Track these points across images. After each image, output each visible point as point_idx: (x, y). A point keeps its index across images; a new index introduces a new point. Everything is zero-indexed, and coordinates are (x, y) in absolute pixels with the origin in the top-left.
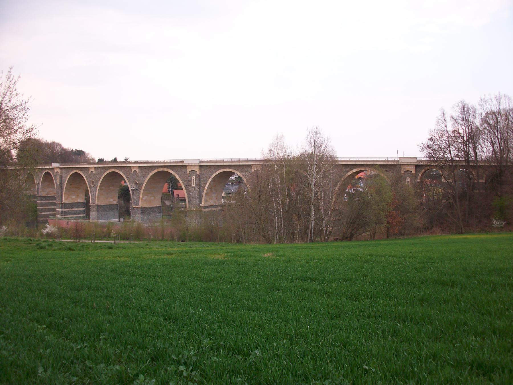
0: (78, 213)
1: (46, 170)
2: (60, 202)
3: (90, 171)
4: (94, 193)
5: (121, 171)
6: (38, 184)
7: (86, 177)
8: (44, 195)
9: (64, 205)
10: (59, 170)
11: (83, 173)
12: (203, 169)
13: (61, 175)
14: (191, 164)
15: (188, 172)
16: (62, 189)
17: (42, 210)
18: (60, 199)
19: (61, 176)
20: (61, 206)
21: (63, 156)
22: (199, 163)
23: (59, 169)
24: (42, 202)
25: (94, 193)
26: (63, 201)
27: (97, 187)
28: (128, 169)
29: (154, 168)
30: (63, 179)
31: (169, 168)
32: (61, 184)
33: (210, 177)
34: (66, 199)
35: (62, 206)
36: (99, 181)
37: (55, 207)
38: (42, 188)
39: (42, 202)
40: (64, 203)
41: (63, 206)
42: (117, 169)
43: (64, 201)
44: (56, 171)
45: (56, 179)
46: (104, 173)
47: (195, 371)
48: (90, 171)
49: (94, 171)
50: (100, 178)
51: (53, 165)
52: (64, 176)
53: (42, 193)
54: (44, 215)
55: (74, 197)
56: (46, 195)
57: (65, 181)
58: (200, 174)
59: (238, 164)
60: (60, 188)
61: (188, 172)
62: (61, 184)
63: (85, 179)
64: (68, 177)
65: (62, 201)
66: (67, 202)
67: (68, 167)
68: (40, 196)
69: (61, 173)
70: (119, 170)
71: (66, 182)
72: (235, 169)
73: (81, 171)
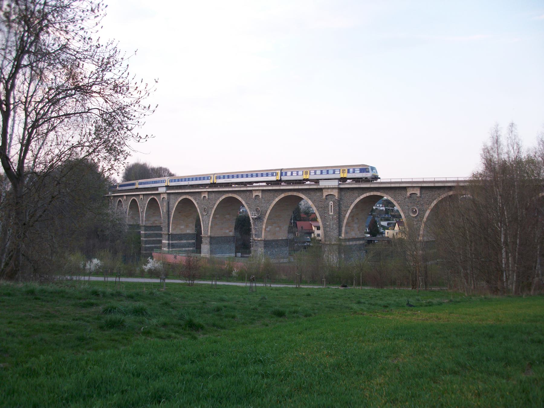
7: (197, 203)
8: (148, 225)
11: (193, 198)
12: (343, 193)
15: (324, 197)
17: (147, 242)
24: (146, 232)
27: (210, 216)
30: (171, 206)
31: (299, 192)
32: (168, 212)
34: (173, 229)
39: (146, 232)
40: (172, 234)
41: (170, 237)
42: (234, 193)
45: (162, 206)
46: (219, 198)
50: (215, 204)
54: (149, 247)
55: (182, 227)
56: (151, 225)
58: (339, 199)
60: (167, 217)
62: (168, 212)
63: (196, 206)
64: (177, 204)
66: (175, 232)
69: (169, 199)
71: (174, 209)
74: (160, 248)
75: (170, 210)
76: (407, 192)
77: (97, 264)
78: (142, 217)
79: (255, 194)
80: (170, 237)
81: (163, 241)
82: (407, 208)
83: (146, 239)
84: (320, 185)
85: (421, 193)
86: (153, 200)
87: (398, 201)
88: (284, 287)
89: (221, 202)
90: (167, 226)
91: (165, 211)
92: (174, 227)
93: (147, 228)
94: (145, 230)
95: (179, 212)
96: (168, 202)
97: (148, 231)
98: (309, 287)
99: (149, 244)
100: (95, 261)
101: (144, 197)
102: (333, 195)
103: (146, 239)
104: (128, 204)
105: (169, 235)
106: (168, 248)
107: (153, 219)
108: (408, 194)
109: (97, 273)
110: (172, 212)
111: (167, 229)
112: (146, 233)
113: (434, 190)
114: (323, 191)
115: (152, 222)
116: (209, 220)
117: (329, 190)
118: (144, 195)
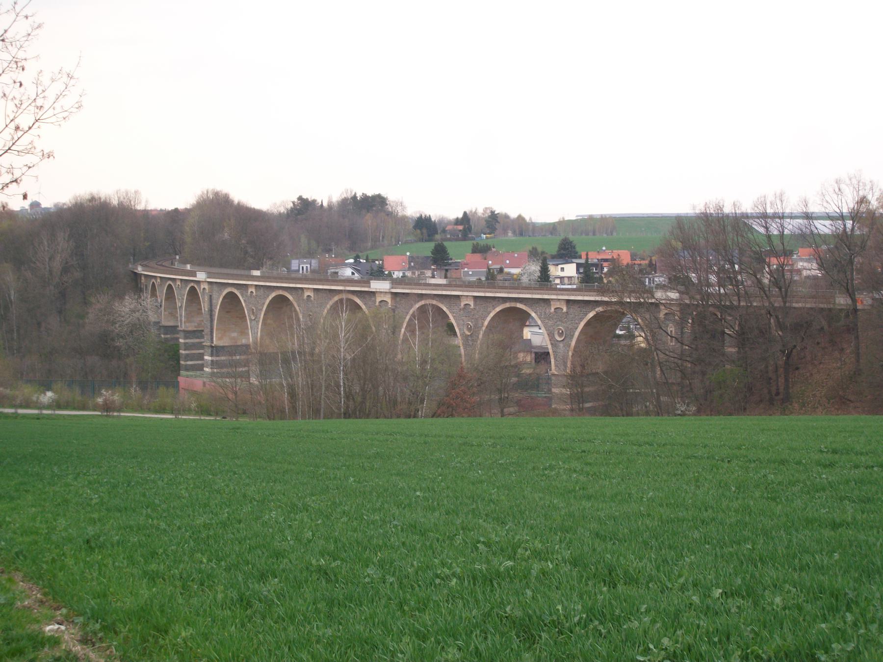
0: (243, 364)
1: (273, 291)
2: (209, 344)
3: (305, 296)
4: (256, 331)
5: (291, 294)
6: (181, 307)
7: (245, 301)
8: (190, 329)
9: (216, 350)
10: (206, 286)
11: (240, 293)
12: (398, 299)
13: (210, 294)
14: (380, 289)
15: (377, 304)
16: (212, 321)
17: (188, 357)
18: (209, 339)
19: (211, 296)
20: (210, 351)
21: (840, 237)
22: (390, 289)
23: (207, 284)
24: (187, 341)
25: (256, 331)
26: (215, 342)
27: (259, 321)
28: (300, 292)
29: (501, 301)
30: (214, 301)
31: (354, 295)
32: (211, 311)
33: (407, 313)
34: (220, 339)
35: (212, 351)
36: (261, 310)
37: (201, 351)
38: (186, 314)
39: (187, 341)
40: (216, 347)
41: (215, 351)
42: (287, 291)
43: (215, 343)
44: (378, 299)
45: (204, 302)
46: (268, 296)
47: (54, 392)
48: (305, 296)
49: (254, 291)
50: (264, 304)
51: (198, 275)
52: (215, 296)
53: (187, 324)
54: (191, 365)
55: (234, 335)
56: (195, 329)
57: (217, 305)
58: (393, 308)
59: (483, 295)
60: (209, 319)
61: (377, 304)
62: (211, 311)
63: (244, 305)
64: (221, 299)
65: (213, 343)
66: (221, 343)
67: (218, 281)
68: (184, 331)
69: (211, 291)
70: (288, 293)
71: (218, 307)
72: (440, 301)
73: (238, 289)
74: (200, 368)
75: (213, 308)
76: (460, 301)
77: (51, 398)
78: (181, 316)
79: (307, 294)
80: (215, 351)
81: (206, 357)
82: (462, 322)
83: (187, 352)
84: (371, 287)
85: (475, 304)
86: (193, 288)
87: (454, 313)
88: (5, 408)
89: (271, 301)
90: (209, 333)
91: (206, 309)
92: (220, 335)
93: (188, 334)
94: (186, 338)
95: (227, 312)
96: (211, 296)
97: (190, 339)
98: (191, 417)
99: (191, 361)
100: (49, 394)
101: (183, 283)
102: (385, 301)
103: (187, 352)
104: (163, 290)
105: (212, 347)
106: (211, 368)
107: (199, 319)
108: (462, 304)
109: (49, 407)
110: (215, 312)
111: (209, 337)
112: (187, 343)
113: (489, 300)
114: (376, 295)
115: (196, 324)
116: (258, 328)
117: (382, 295)
118: (181, 280)
